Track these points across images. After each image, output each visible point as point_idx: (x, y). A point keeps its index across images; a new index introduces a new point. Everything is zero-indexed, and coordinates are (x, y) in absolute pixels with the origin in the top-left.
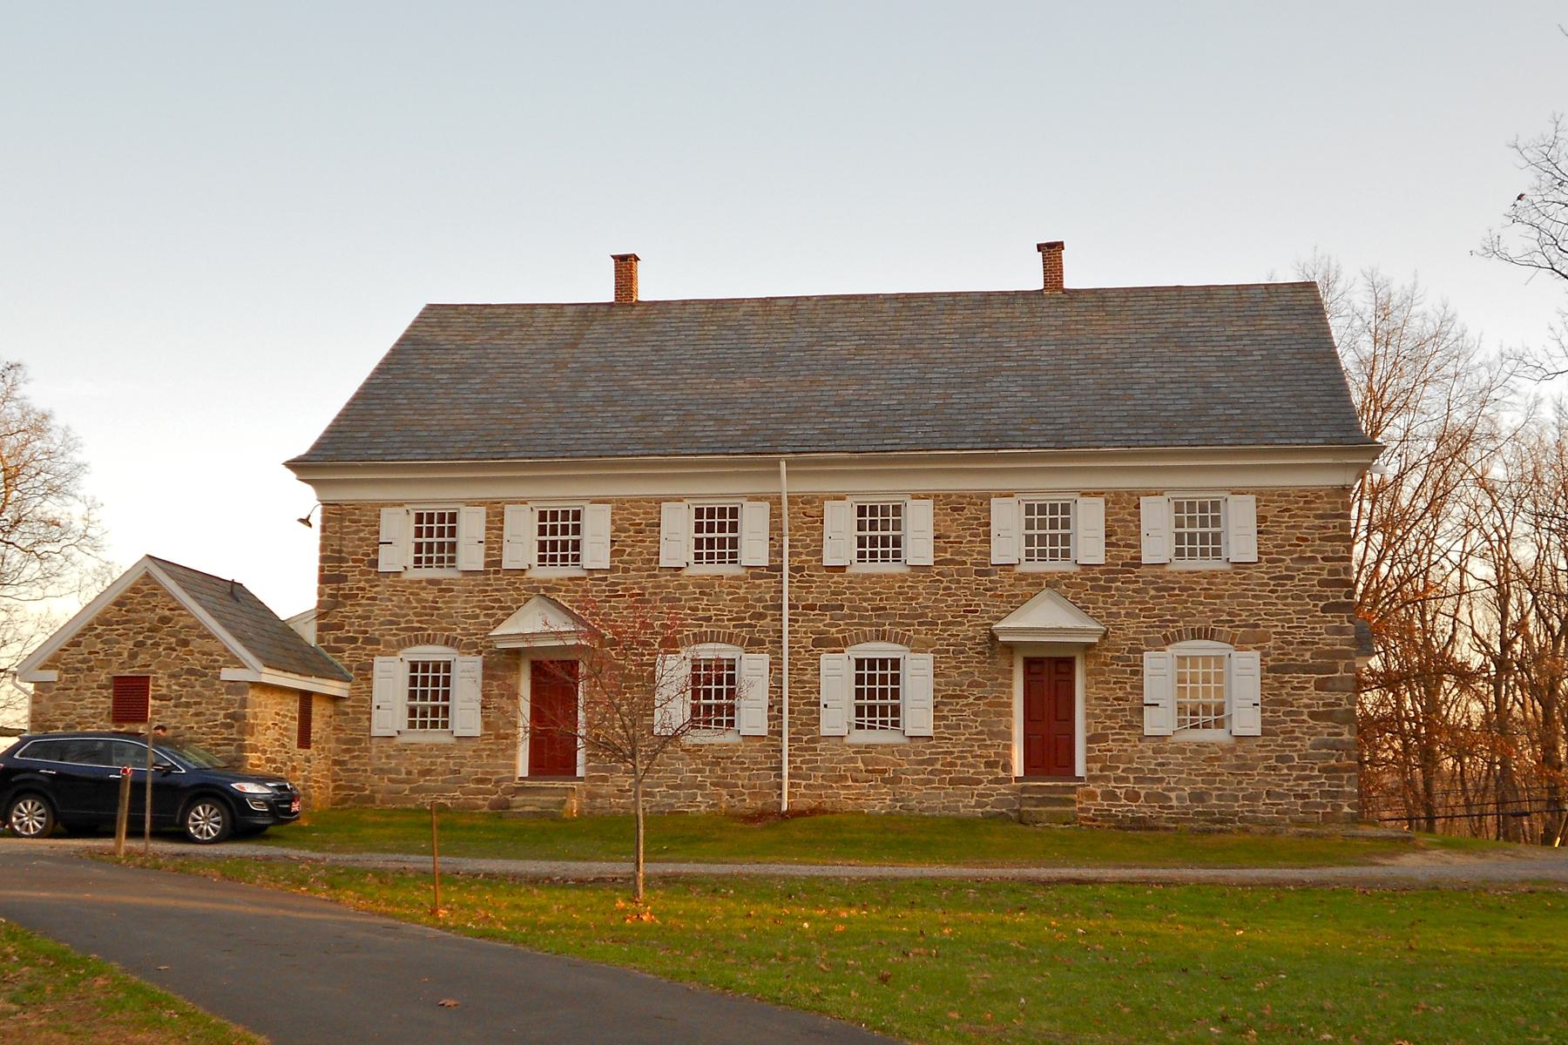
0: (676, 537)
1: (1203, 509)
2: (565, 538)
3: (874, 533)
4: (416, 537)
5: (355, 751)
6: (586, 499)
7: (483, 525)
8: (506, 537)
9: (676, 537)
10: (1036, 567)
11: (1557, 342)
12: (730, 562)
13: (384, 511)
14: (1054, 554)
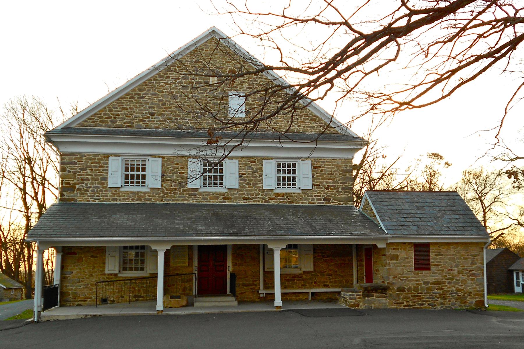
0: (270, 176)
1: (289, 166)
2: (289, 175)
3: (138, 173)
4: (125, 171)
5: (437, 259)
6: (298, 158)
7: (110, 165)
8: (110, 172)
9: (270, 176)
10: (281, 191)
11: (337, 102)
12: (219, 186)
13: (265, 161)
14: (284, 185)
